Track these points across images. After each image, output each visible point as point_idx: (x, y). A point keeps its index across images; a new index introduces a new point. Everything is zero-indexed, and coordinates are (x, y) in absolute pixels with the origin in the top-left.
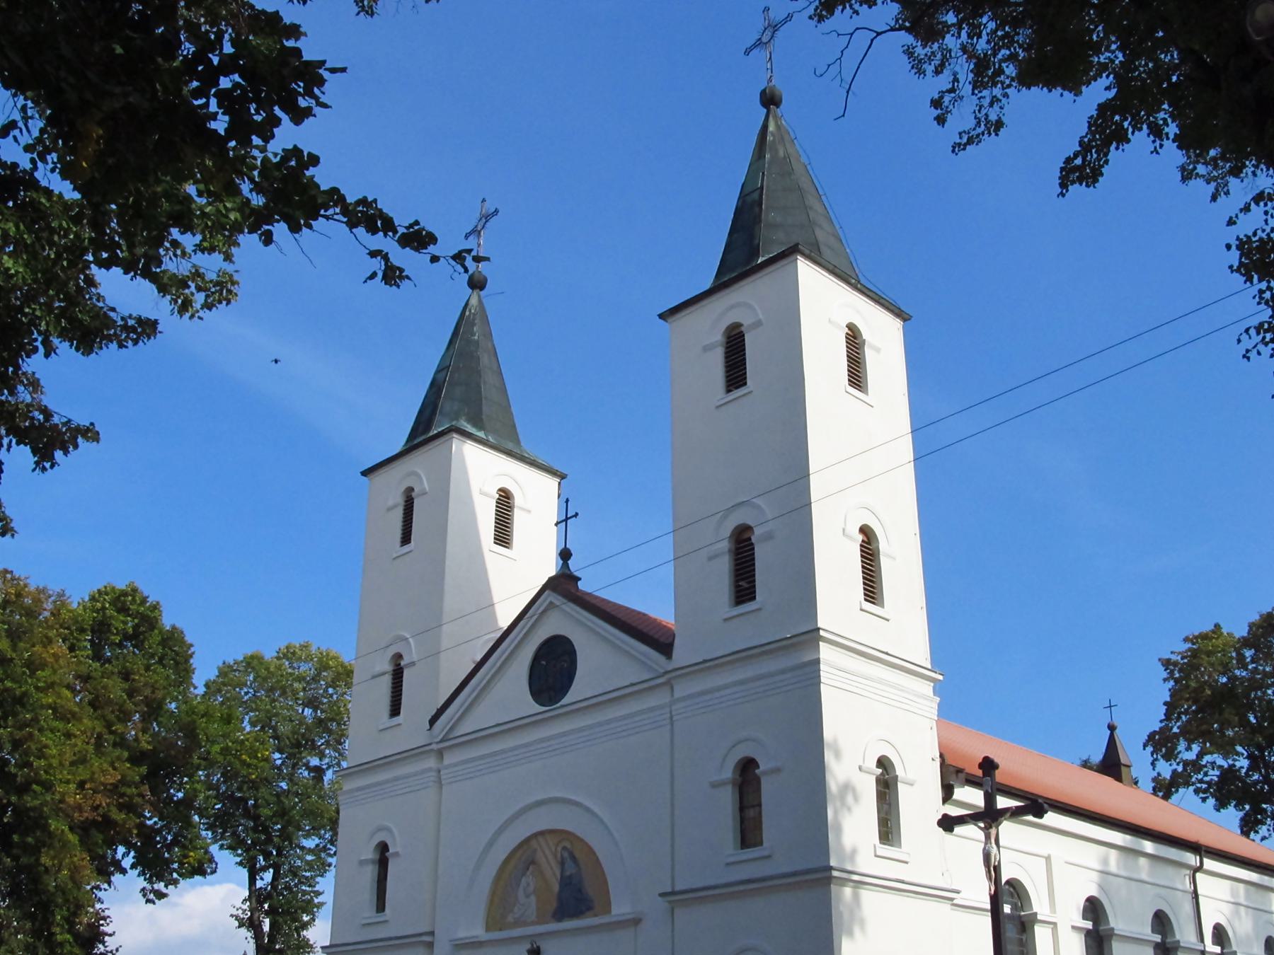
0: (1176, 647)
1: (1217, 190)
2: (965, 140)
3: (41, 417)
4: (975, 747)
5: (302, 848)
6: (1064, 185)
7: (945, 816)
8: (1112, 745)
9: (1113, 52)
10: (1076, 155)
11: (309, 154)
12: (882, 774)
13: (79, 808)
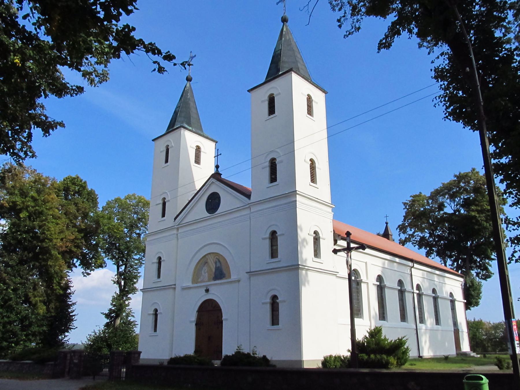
0: (408, 199)
1: (430, 51)
2: (348, 33)
3: (44, 118)
4: (344, 229)
5: (134, 259)
6: (379, 49)
7: (335, 249)
8: (386, 229)
9: (398, 4)
10: (383, 39)
11: (132, 27)
12: (315, 236)
13: (61, 247)
